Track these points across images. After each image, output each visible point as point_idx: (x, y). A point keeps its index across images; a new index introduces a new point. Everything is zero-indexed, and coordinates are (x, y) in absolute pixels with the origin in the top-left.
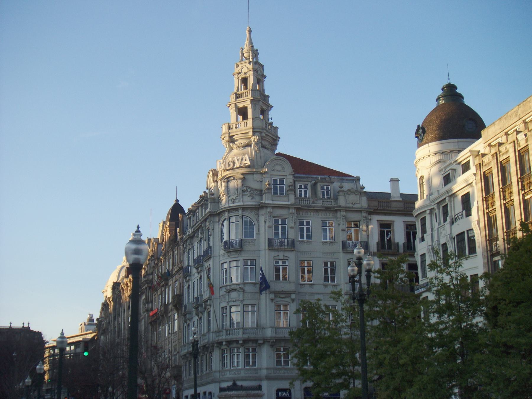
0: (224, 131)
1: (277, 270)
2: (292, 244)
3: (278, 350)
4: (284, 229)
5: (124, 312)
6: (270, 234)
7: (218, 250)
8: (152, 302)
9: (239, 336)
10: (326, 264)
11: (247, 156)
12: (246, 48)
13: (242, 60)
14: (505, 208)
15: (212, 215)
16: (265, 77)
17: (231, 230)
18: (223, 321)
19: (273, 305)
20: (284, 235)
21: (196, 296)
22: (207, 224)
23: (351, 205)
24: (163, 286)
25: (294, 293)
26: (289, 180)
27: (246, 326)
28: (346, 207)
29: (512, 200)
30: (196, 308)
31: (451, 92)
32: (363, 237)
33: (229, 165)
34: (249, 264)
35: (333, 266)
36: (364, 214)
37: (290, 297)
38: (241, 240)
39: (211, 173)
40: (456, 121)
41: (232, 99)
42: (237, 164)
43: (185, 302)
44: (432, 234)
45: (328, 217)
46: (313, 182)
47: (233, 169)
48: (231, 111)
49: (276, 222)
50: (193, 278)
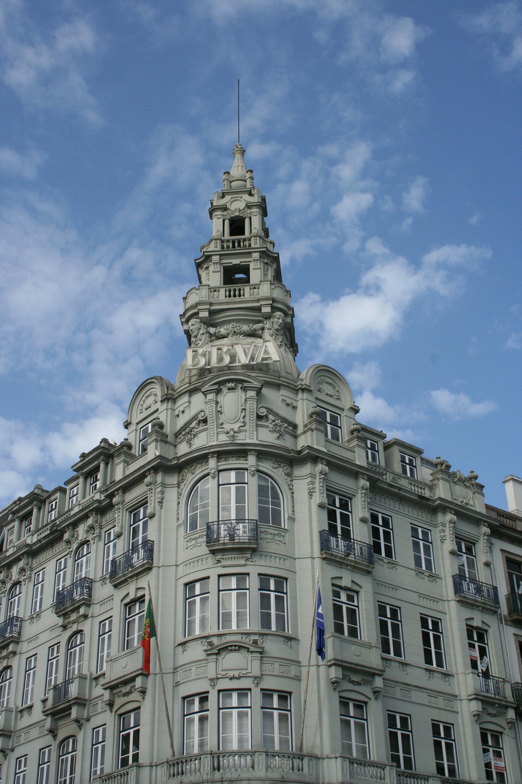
1: (337, 610)
34: (272, 588)
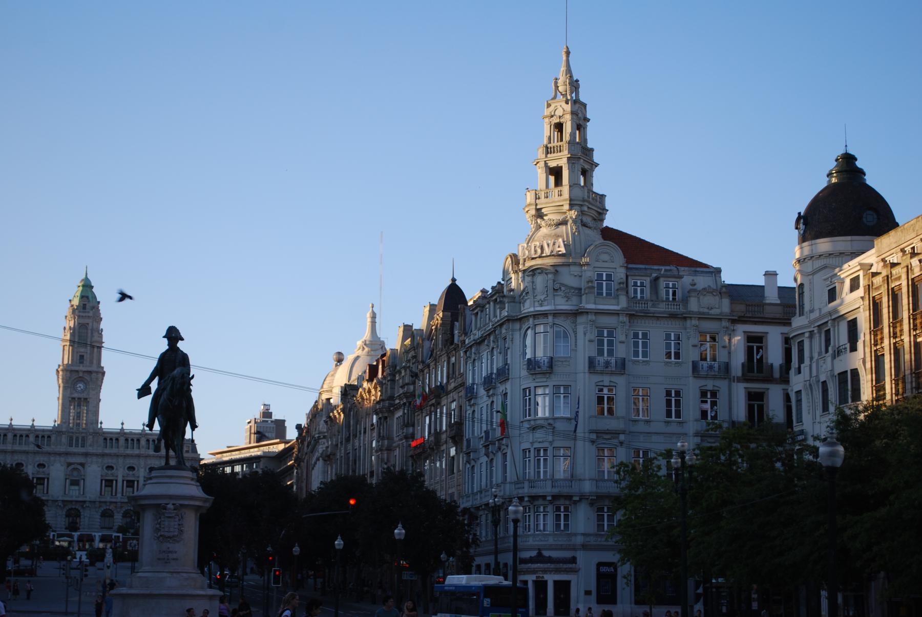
0: (528, 201)
2: (622, 365)
3: (600, 509)
4: (610, 343)
5: (365, 432)
6: (592, 351)
7: (519, 370)
8: (413, 426)
9: (547, 489)
10: (668, 393)
11: (560, 240)
12: (562, 78)
13: (555, 98)
14: (895, 348)
15: (510, 320)
16: (588, 120)
17: (536, 344)
18: (525, 468)
19: (593, 448)
20: (610, 353)
21: (484, 428)
22: (504, 331)
23: (706, 310)
24: (433, 405)
25: (623, 432)
26: (620, 273)
27: (557, 477)
28: (700, 313)
29: (902, 340)
30: (486, 447)
31: (848, 165)
32: (722, 357)
33: (536, 251)
35: (679, 396)
36: (725, 323)
37: (618, 438)
38: (552, 358)
39: (509, 259)
40: (848, 209)
41: (541, 154)
42: (547, 251)
43: (467, 434)
44: (811, 366)
45: (673, 327)
46: (654, 275)
47: (540, 257)
48: (539, 171)
49: (600, 334)
50: (479, 401)
